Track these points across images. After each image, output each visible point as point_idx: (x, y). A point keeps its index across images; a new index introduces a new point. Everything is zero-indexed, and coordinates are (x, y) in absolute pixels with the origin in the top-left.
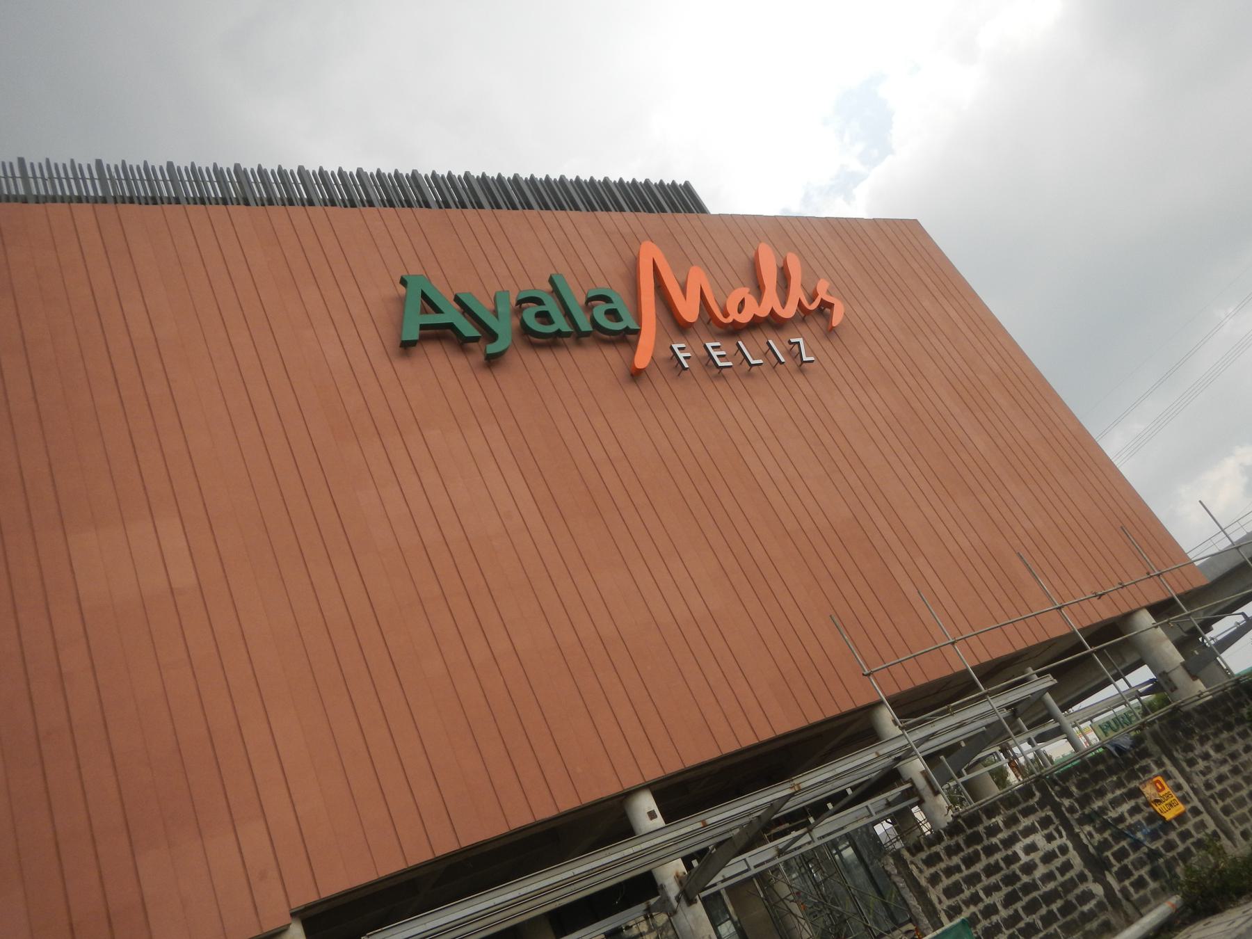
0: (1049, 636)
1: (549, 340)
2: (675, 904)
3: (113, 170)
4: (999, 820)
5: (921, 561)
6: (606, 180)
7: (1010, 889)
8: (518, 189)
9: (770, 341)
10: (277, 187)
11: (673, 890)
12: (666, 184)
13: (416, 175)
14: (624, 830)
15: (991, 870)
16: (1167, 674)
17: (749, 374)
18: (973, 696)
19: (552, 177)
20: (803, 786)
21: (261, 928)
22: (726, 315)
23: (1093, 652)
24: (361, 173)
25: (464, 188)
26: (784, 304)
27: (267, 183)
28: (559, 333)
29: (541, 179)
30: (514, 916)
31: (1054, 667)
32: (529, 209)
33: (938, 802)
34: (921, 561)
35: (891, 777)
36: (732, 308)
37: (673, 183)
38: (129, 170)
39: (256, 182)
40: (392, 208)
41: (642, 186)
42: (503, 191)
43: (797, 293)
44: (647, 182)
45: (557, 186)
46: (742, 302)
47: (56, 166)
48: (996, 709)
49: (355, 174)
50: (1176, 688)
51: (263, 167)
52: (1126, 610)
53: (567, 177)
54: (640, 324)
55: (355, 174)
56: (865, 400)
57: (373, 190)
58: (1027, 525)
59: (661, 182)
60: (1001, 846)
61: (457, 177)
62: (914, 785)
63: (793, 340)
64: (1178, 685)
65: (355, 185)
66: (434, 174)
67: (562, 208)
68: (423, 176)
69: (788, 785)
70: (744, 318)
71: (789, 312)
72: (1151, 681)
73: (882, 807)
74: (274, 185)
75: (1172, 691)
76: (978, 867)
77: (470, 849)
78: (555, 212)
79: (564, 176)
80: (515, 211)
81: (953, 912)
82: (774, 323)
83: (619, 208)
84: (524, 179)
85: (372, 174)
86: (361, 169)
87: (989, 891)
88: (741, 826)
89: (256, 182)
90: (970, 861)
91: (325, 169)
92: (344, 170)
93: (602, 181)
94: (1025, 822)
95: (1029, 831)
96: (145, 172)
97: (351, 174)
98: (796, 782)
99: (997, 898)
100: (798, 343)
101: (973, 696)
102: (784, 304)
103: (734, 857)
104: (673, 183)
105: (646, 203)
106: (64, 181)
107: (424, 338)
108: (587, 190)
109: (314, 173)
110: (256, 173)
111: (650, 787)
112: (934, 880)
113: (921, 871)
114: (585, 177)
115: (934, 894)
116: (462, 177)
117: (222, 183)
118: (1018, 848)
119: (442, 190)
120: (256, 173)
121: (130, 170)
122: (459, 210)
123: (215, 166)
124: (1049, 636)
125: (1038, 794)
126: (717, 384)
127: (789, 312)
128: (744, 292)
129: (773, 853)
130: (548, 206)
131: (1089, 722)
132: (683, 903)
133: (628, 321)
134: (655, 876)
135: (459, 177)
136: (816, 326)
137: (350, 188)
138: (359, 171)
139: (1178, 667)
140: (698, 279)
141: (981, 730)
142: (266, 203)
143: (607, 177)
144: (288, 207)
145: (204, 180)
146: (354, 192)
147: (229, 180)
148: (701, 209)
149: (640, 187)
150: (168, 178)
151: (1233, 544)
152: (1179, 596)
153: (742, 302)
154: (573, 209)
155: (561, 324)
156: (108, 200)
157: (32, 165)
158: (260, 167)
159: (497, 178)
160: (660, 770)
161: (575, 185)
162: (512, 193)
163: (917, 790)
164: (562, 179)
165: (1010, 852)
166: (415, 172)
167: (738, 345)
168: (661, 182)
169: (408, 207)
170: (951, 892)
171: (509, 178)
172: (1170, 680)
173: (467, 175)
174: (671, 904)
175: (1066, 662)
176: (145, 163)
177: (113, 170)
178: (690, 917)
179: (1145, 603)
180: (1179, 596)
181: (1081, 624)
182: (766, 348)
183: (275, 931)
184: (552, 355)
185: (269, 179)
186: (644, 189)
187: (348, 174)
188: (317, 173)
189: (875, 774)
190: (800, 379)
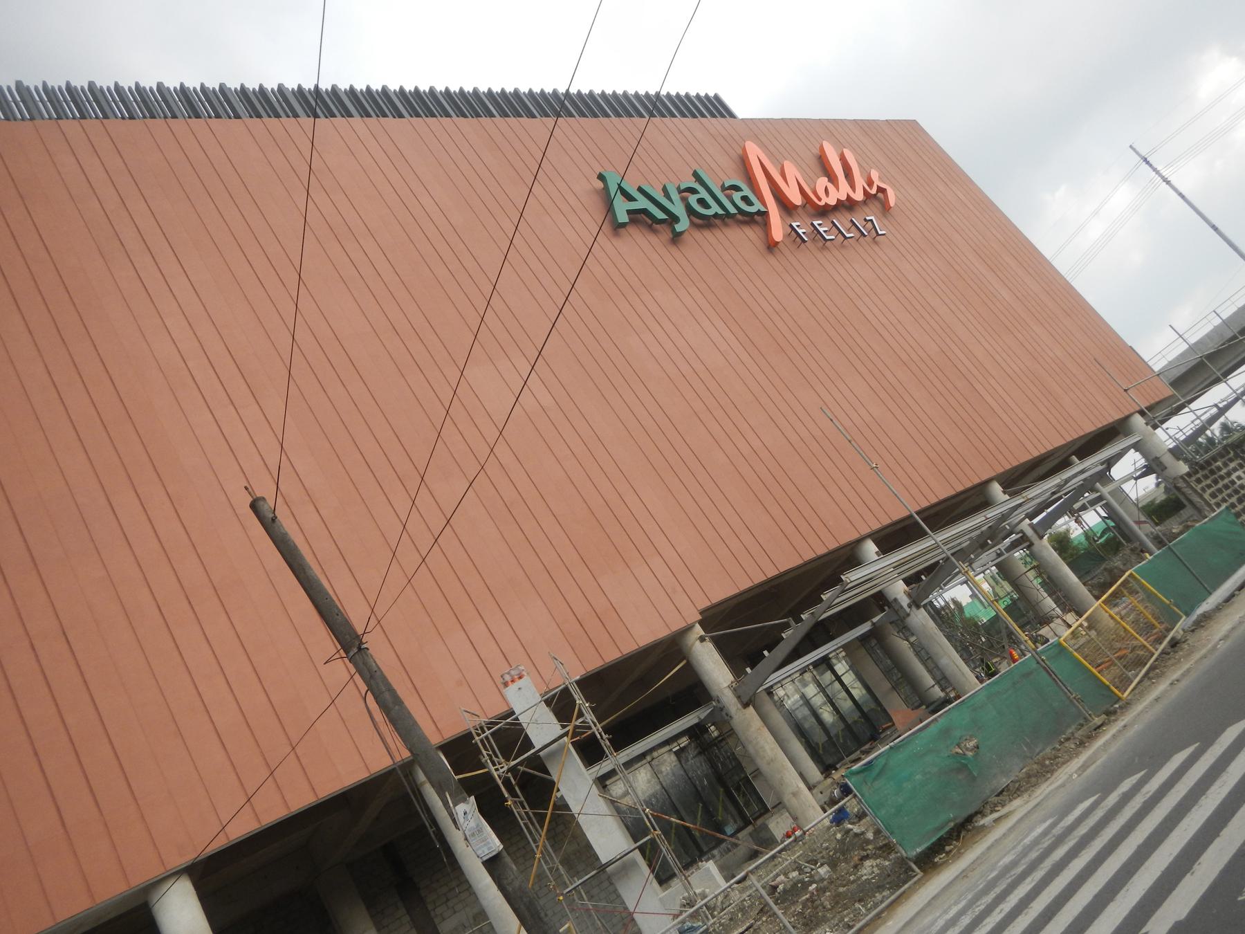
0: (1065, 440)
1: (746, 218)
2: (908, 610)
4: (1219, 463)
5: (993, 382)
6: (385, 90)
7: (1238, 496)
8: (466, 103)
9: (834, 220)
10: (116, 105)
11: (905, 601)
12: (508, 92)
14: (987, 503)
15: (1226, 487)
16: (1159, 458)
17: (824, 248)
19: (547, 91)
20: (1029, 497)
21: (288, 808)
22: (820, 199)
23: (1185, 402)
24: (162, 89)
25: (278, 101)
26: (854, 190)
27: (55, 100)
28: (716, 215)
29: (309, 89)
30: (927, 560)
32: (383, 117)
33: (1043, 544)
34: (993, 382)
35: (992, 535)
36: (821, 193)
37: (416, 89)
38: (58, 92)
39: (42, 100)
41: (550, 95)
42: (405, 102)
43: (860, 182)
44: (384, 89)
45: (428, 98)
46: (826, 188)
48: (940, 544)
49: (155, 89)
50: (1166, 468)
52: (1127, 413)
54: (767, 209)
55: (155, 89)
56: (923, 264)
58: (1051, 354)
59: (402, 89)
60: (1238, 468)
61: (192, 89)
62: (1024, 534)
63: (868, 218)
64: (1167, 465)
65: (157, 100)
67: (433, 115)
69: (1020, 497)
70: (832, 202)
71: (858, 196)
72: (1145, 466)
73: (995, 557)
74: (40, 104)
75: (1162, 470)
76: (1220, 485)
77: (719, 604)
78: (426, 119)
79: (386, 86)
80: (534, 119)
81: (1218, 505)
82: (848, 205)
83: (503, 114)
84: (393, 91)
86: (162, 83)
87: (1230, 496)
88: (970, 539)
89: (42, 100)
90: (1216, 482)
92: (207, 86)
94: (1232, 465)
95: (1235, 470)
96: (18, 93)
97: (195, 89)
98: (1024, 495)
99: (1234, 500)
100: (871, 220)
102: (854, 190)
103: (774, 672)
104: (416, 89)
105: (567, 109)
107: (633, 221)
108: (412, 100)
109: (130, 89)
111: (869, 536)
112: (1203, 490)
113: (1196, 486)
114: (496, 89)
115: (1207, 496)
116: (276, 89)
118: (1234, 477)
119: (254, 105)
121: (60, 92)
122: (475, 119)
123: (45, 84)
124: (1065, 440)
125: (1232, 452)
126: (825, 253)
127: (858, 196)
128: (823, 182)
129: (994, 555)
130: (493, 113)
131: (982, 575)
132: (914, 608)
133: (757, 206)
135: (272, 90)
136: (875, 206)
137: (195, 104)
138: (222, 86)
139: (1166, 453)
140: (792, 171)
141: (1080, 483)
143: (335, 85)
144: (170, 121)
145: (58, 101)
146: (200, 109)
148: (732, 115)
149: (510, 96)
152: (1146, 408)
153: (826, 188)
155: (715, 209)
158: (116, 84)
159: (429, 91)
160: (918, 506)
161: (445, 96)
163: (1027, 537)
165: (1230, 479)
166: (160, 85)
167: (833, 222)
168: (402, 89)
169: (275, 117)
170: (1213, 496)
171: (327, 90)
172: (1161, 463)
174: (905, 610)
175: (738, 632)
178: (920, 616)
180: (1146, 408)
182: (850, 225)
183: (155, 880)
184: (711, 234)
186: (514, 99)
188: (172, 90)
189: (1032, 509)
190: (876, 248)
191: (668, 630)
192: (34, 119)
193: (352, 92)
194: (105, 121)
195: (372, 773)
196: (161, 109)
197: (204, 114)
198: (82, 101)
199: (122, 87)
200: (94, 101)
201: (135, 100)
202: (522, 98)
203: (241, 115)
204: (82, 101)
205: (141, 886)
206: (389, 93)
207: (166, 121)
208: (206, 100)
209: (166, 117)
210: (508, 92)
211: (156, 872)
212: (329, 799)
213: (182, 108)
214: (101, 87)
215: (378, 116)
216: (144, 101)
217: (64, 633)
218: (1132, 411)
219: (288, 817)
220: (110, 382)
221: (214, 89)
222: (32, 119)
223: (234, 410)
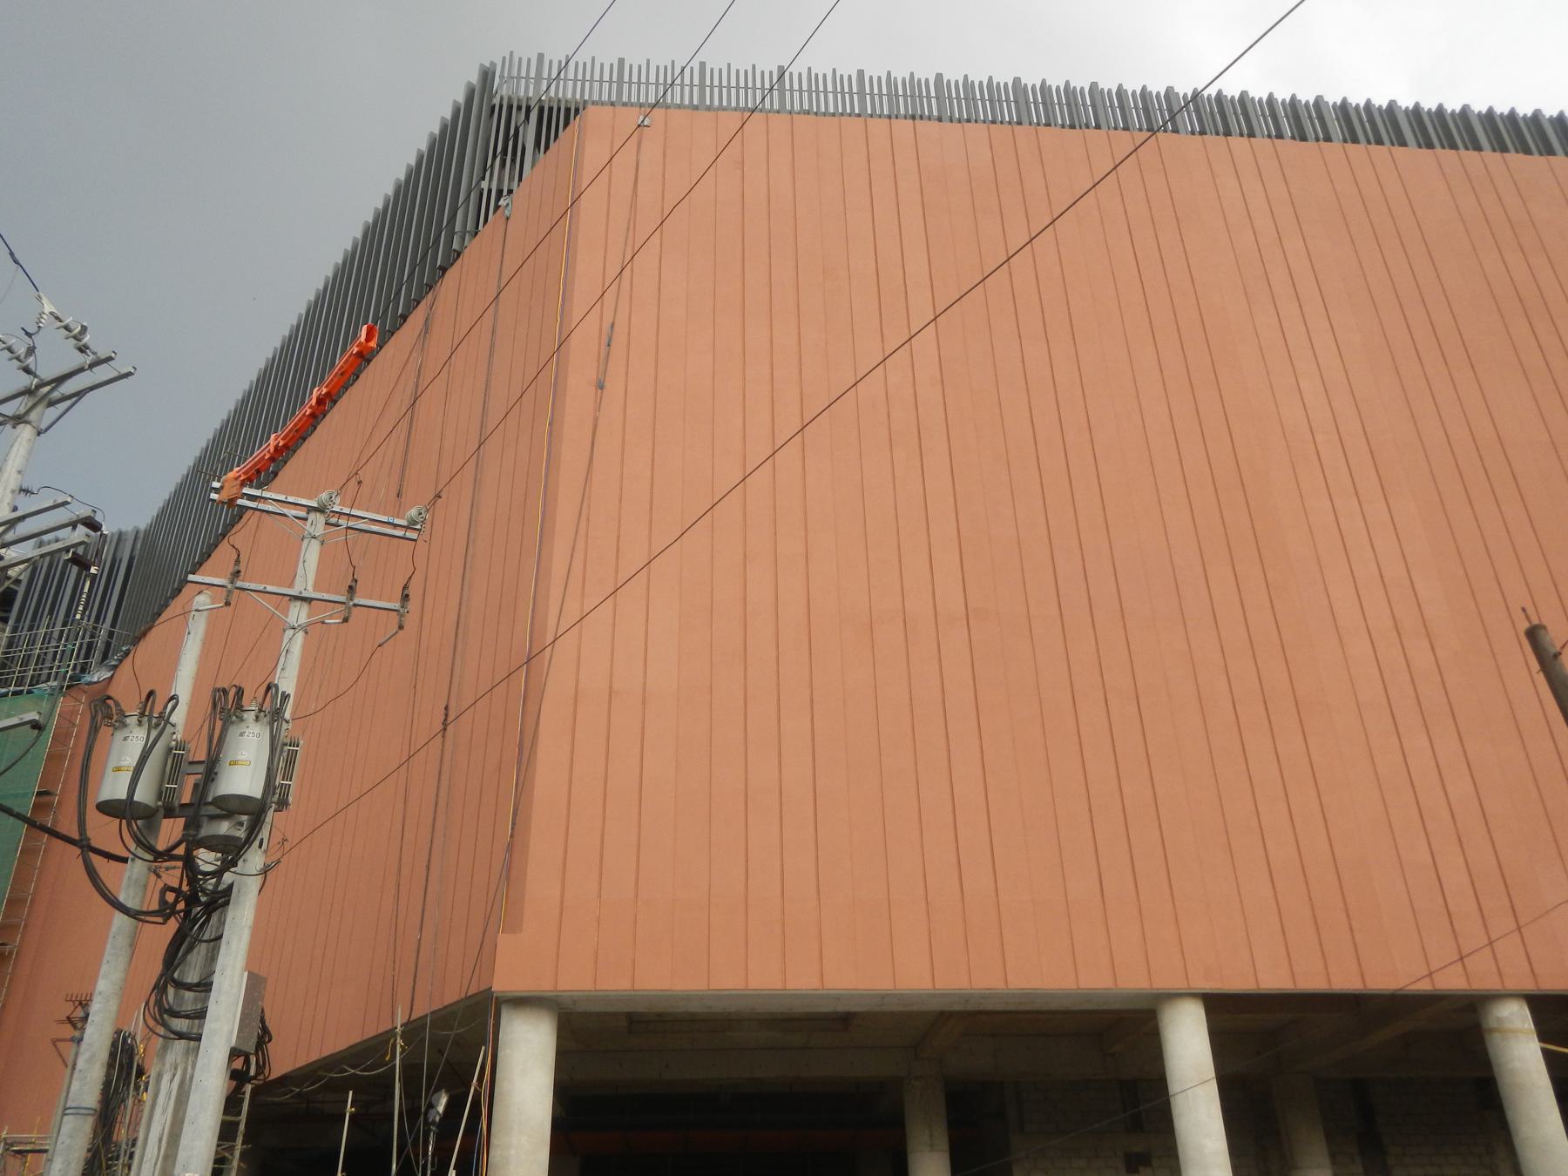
3: (923, 82)
10: (1060, 109)
13: (1395, 108)
18: (354, 271)
31: (392, 1154)
40: (1453, 151)
42: (1391, 124)
47: (842, 76)
51: (1149, 90)
53: (1472, 108)
57: (1259, 121)
66: (1368, 103)
67: (1453, 146)
68: (1280, 101)
85: (1260, 100)
91: (1125, 88)
93: (1384, 107)
101: (354, 271)
106: (847, 96)
109: (1134, 93)
110: (1038, 90)
116: (1265, 100)
117: (1073, 105)
120: (1038, 90)
134: (1173, 1111)
142: (1083, 126)
143: (1395, 101)
147: (1032, 100)
150: (987, 98)
151: (935, 988)
154: (1423, 146)
156: (943, 119)
157: (871, 78)
162: (1505, 135)
164: (1465, 110)
173: (1368, 104)
176: (990, 78)
177: (923, 82)
179: (1529, 986)
181: (1469, 983)
185: (1052, 97)
187: (1280, 102)
191: (1186, 984)
192: (1230, 135)
193: (1344, 108)
194: (1278, 142)
195: (711, 988)
196: (1078, 114)
197: (1186, 127)
198: (1076, 105)
199: (1276, 99)
200: (1368, 121)
201: (1136, 107)
202: (1496, 122)
203: (1332, 137)
204: (1076, 105)
205: (1066, 991)
206: (1396, 112)
207: (1343, 147)
208: (1119, 107)
209: (1345, 141)
210: (1521, 115)
211: (1179, 984)
212: (793, 995)
213: (1335, 128)
214: (1102, 89)
215: (1369, 142)
216: (1146, 109)
217: (1137, 698)
218: (1512, 985)
219: (1532, 993)
220: (1229, 440)
221: (1358, 105)
222: (1098, 127)
223: (1356, 503)
